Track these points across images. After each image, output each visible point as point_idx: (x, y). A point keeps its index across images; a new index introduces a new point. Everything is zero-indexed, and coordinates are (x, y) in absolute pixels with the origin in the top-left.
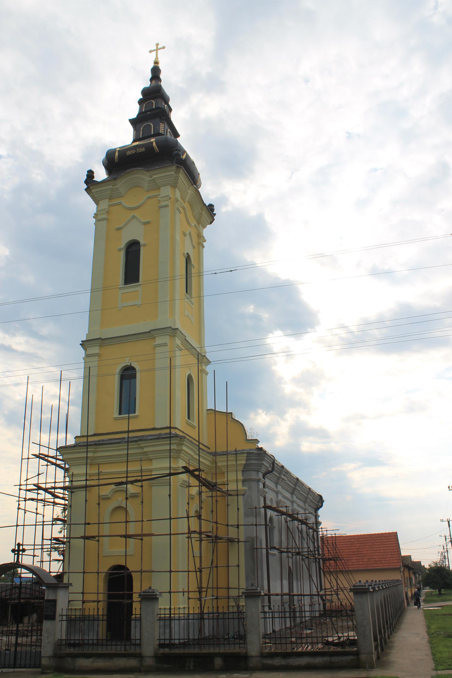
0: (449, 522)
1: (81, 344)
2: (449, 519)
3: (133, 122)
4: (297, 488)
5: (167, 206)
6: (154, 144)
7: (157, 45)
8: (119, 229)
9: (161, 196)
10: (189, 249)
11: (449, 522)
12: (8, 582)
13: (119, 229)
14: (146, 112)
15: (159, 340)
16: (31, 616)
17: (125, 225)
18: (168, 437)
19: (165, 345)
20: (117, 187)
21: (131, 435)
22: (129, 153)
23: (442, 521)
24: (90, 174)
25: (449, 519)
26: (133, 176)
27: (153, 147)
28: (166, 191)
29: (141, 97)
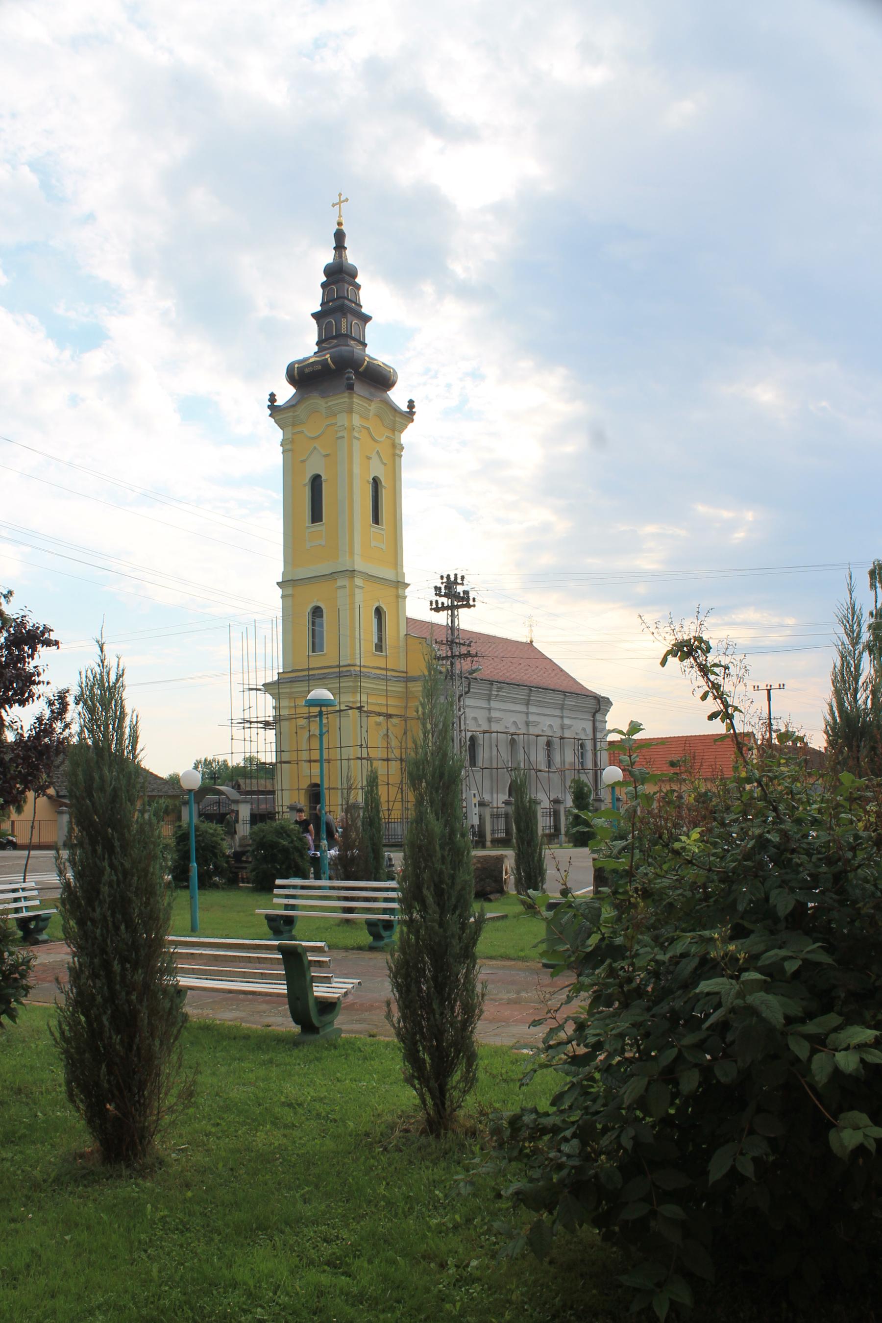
0: (769, 691)
1: (278, 583)
2: (771, 686)
4: (531, 698)
6: (329, 359)
7: (340, 195)
8: (303, 461)
9: (338, 425)
10: (377, 470)
11: (769, 691)
13: (303, 461)
14: (328, 302)
15: (340, 582)
18: (306, 680)
20: (296, 414)
21: (311, 672)
22: (307, 371)
23: (756, 688)
24: (272, 398)
25: (771, 686)
26: (312, 401)
27: (328, 364)
28: (342, 419)
29: (325, 279)
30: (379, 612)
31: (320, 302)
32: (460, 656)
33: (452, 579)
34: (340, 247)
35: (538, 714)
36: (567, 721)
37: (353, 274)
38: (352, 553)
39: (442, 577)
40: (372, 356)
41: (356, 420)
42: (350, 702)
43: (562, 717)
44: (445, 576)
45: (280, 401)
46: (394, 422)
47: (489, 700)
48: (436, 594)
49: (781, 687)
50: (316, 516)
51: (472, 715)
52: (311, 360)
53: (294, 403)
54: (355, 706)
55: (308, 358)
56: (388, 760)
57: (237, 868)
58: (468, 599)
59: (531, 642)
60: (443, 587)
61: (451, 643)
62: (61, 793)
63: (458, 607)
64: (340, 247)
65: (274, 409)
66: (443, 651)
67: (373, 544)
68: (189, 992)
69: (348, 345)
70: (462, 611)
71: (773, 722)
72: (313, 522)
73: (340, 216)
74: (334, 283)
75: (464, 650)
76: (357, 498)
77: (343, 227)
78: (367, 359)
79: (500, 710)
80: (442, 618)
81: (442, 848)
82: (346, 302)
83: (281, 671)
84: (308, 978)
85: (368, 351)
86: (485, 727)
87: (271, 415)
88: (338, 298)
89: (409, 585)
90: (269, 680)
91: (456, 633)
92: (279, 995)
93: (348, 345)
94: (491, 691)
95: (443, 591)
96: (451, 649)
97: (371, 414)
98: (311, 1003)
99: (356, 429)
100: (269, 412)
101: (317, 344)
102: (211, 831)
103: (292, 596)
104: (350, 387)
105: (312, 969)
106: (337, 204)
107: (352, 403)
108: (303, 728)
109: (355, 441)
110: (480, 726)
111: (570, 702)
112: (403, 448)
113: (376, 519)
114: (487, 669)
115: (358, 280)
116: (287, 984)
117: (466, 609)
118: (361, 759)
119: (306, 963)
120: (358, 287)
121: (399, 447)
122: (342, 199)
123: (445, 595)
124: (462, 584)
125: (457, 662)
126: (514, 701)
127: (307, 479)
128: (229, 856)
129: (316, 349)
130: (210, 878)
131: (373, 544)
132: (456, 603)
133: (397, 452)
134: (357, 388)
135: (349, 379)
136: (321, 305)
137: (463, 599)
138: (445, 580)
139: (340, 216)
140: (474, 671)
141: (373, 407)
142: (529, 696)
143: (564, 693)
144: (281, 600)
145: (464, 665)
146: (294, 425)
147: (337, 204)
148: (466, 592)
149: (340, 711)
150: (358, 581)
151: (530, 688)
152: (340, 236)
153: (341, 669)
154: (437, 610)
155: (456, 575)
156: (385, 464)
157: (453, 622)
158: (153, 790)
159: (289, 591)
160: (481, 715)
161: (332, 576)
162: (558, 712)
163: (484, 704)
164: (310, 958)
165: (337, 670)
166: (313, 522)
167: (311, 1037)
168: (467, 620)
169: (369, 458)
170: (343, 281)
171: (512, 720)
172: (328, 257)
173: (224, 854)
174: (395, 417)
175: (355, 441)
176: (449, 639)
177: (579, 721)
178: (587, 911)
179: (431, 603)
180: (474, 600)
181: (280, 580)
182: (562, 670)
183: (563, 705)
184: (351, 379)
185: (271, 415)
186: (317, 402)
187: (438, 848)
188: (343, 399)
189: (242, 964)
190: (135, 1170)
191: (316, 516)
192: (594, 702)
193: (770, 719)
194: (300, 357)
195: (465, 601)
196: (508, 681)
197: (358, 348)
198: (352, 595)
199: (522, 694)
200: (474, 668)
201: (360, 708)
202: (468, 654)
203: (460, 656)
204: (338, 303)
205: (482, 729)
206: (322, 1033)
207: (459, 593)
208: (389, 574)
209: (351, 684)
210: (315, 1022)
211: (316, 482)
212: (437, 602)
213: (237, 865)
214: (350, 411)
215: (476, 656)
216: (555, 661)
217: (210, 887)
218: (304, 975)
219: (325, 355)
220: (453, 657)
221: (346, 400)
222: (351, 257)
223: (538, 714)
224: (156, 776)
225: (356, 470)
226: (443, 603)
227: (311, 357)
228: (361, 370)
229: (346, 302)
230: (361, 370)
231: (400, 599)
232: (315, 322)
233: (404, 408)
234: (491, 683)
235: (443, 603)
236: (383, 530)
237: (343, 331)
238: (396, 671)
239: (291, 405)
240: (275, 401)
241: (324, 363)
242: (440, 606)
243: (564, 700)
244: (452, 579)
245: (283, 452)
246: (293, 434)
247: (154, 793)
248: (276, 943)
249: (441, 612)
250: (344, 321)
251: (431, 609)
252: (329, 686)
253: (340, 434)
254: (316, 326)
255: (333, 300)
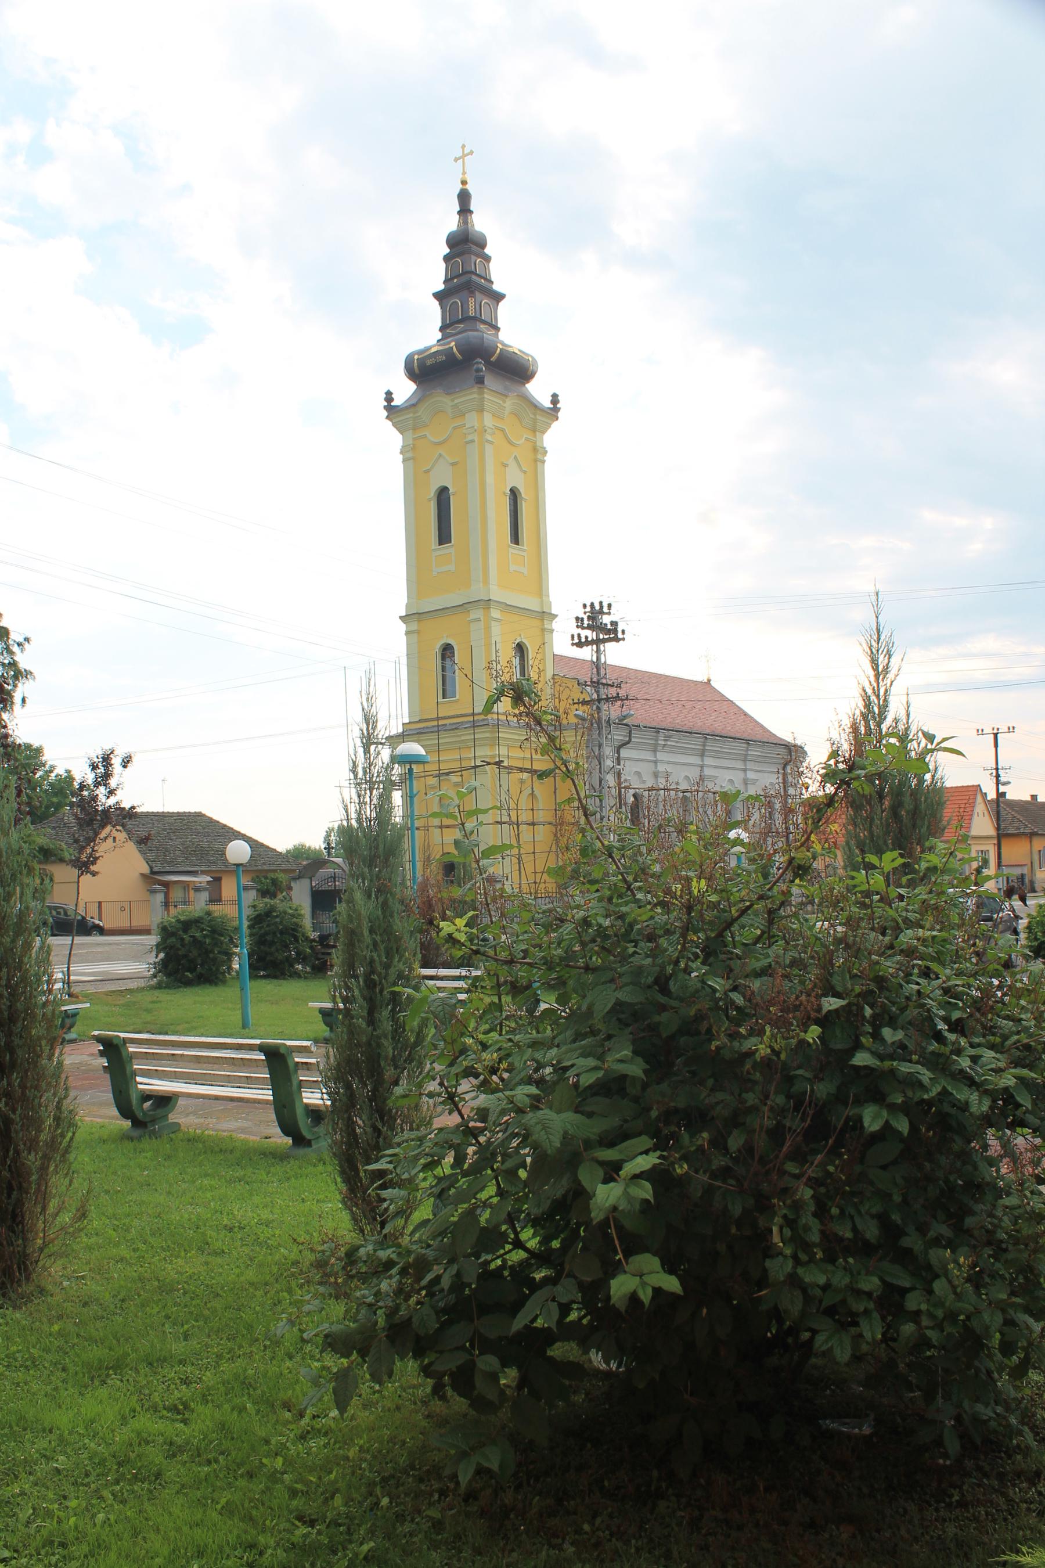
0: (996, 735)
1: (401, 618)
3: (439, 296)
5: (473, 441)
7: (463, 147)
8: (427, 472)
10: (515, 478)
11: (996, 735)
12: (166, 1034)
13: (427, 472)
14: (452, 279)
15: (473, 615)
16: (140, 1086)
17: (432, 467)
19: (478, 620)
22: (429, 362)
24: (389, 396)
27: (453, 354)
28: (472, 420)
29: (448, 250)
30: (520, 649)
31: (443, 279)
32: (607, 699)
33: (597, 607)
34: (465, 211)
35: (716, 767)
36: (751, 775)
37: (482, 243)
38: (486, 581)
39: (585, 606)
40: (507, 342)
41: (489, 420)
42: (487, 756)
43: (745, 770)
44: (588, 604)
45: (398, 401)
46: (535, 420)
47: (655, 751)
48: (578, 626)
49: (1011, 730)
50: (444, 536)
51: (635, 769)
52: (433, 350)
53: (413, 401)
54: (492, 761)
55: (430, 348)
56: (533, 824)
57: (323, 954)
58: (615, 631)
59: (709, 680)
60: (585, 617)
61: (596, 684)
62: (156, 869)
63: (604, 641)
64: (465, 211)
65: (391, 409)
66: (590, 693)
67: (512, 567)
68: (181, 1102)
69: (477, 330)
70: (610, 647)
71: (1001, 772)
72: (440, 544)
73: (464, 173)
74: (459, 255)
75: (612, 692)
76: (491, 514)
77: (468, 187)
78: (500, 346)
79: (669, 763)
80: (587, 653)
81: (372, 931)
82: (474, 277)
83: (406, 720)
84: (295, 1083)
85: (502, 336)
86: (649, 784)
87: (387, 418)
88: (464, 273)
89: (556, 616)
90: (394, 732)
91: (602, 672)
92: (267, 1102)
93: (477, 330)
94: (657, 740)
95: (586, 622)
96: (597, 692)
97: (507, 412)
98: (300, 1112)
99: (489, 430)
100: (386, 414)
101: (441, 329)
102: (290, 911)
103: (418, 632)
104: (480, 381)
105: (299, 1072)
106: (459, 158)
107: (482, 400)
108: (433, 788)
109: (487, 445)
110: (644, 782)
111: (754, 752)
112: (546, 452)
113: (516, 539)
114: (639, 713)
115: (487, 251)
116: (272, 1089)
117: (614, 643)
118: (501, 823)
119: (291, 1065)
120: (488, 259)
121: (541, 450)
122: (466, 152)
123: (589, 627)
124: (609, 613)
125: (605, 707)
126: (686, 751)
127: (432, 493)
128: (314, 940)
129: (439, 336)
130: (292, 966)
131: (512, 567)
132: (601, 636)
133: (539, 456)
134: (489, 380)
135: (479, 370)
136: (444, 282)
137: (609, 632)
138: (588, 609)
139: (464, 173)
140: (625, 717)
141: (509, 404)
142: (704, 746)
143: (747, 741)
144: (404, 638)
145: (613, 711)
146: (415, 429)
147: (459, 158)
148: (614, 624)
149: (476, 767)
150: (495, 613)
151: (705, 736)
152: (464, 198)
153: (476, 718)
154: (580, 645)
155: (601, 603)
156: (525, 472)
157: (598, 658)
158: (264, 863)
159: (414, 626)
160: (646, 769)
161: (464, 607)
162: (740, 765)
163: (649, 756)
164: (297, 1060)
165: (471, 719)
166: (440, 544)
167: (301, 1151)
168: (614, 654)
169: (505, 466)
170: (470, 252)
171: (683, 775)
172: (452, 223)
173: (307, 938)
174: (535, 415)
175: (487, 445)
176: (595, 680)
177: (766, 775)
178: (440, 1008)
179: (573, 637)
180: (623, 632)
181: (404, 614)
182: (745, 714)
183: (746, 755)
184: (481, 370)
185: (387, 418)
186: (442, 399)
187: (366, 933)
188: (471, 395)
189: (216, 1066)
190: (10, 1299)
191: (444, 536)
192: (783, 751)
193: (997, 769)
194: (420, 346)
195: (612, 633)
196: (678, 728)
197: (488, 334)
198: (488, 629)
199: (696, 743)
200: (624, 714)
201: (499, 763)
202: (617, 698)
203: (607, 699)
204: (464, 279)
205: (646, 786)
206: (314, 1146)
207: (606, 625)
208: (532, 604)
209: (488, 735)
210: (306, 1133)
211: (443, 496)
212: (579, 636)
213: (323, 951)
214: (481, 410)
215: (627, 699)
216: (738, 703)
217: (290, 976)
218: (290, 1080)
219: (449, 343)
220: (599, 700)
221: (476, 396)
222: (480, 223)
223: (716, 767)
224: (268, 847)
225: (490, 479)
226: (586, 637)
227: (434, 346)
228: (493, 359)
229: (474, 277)
230: (493, 359)
231: (545, 632)
232: (437, 303)
233: (547, 403)
234: (657, 730)
235: (586, 637)
236: (524, 551)
237: (471, 313)
238: (426, 720)
239: (412, 405)
240: (392, 400)
241: (449, 353)
242: (583, 640)
243: (747, 750)
244: (597, 607)
245: (404, 461)
246: (414, 439)
247: (265, 867)
248: (258, 1042)
249: (585, 648)
250: (471, 301)
251: (573, 644)
252: (424, 743)
253: (469, 438)
254: (439, 308)
255: (458, 276)
